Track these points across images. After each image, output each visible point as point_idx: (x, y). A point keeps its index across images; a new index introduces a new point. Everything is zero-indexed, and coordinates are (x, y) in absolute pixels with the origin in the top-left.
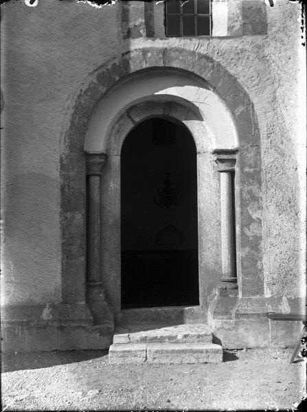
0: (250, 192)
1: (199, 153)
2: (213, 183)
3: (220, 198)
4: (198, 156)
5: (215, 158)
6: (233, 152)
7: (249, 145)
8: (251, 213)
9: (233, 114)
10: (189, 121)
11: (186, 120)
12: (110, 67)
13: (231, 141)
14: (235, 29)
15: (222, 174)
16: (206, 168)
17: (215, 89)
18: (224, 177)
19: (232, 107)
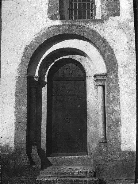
0: (113, 96)
1: (88, 77)
2: (94, 92)
3: (98, 100)
4: (87, 78)
5: (95, 79)
6: (106, 75)
7: (112, 72)
8: (114, 106)
9: (104, 57)
10: (44, 149)
11: (44, 151)
12: (41, 34)
13: (102, 69)
14: (104, 16)
15: (99, 87)
16: (90, 83)
17: (95, 45)
18: (100, 88)
19: (102, 54)
